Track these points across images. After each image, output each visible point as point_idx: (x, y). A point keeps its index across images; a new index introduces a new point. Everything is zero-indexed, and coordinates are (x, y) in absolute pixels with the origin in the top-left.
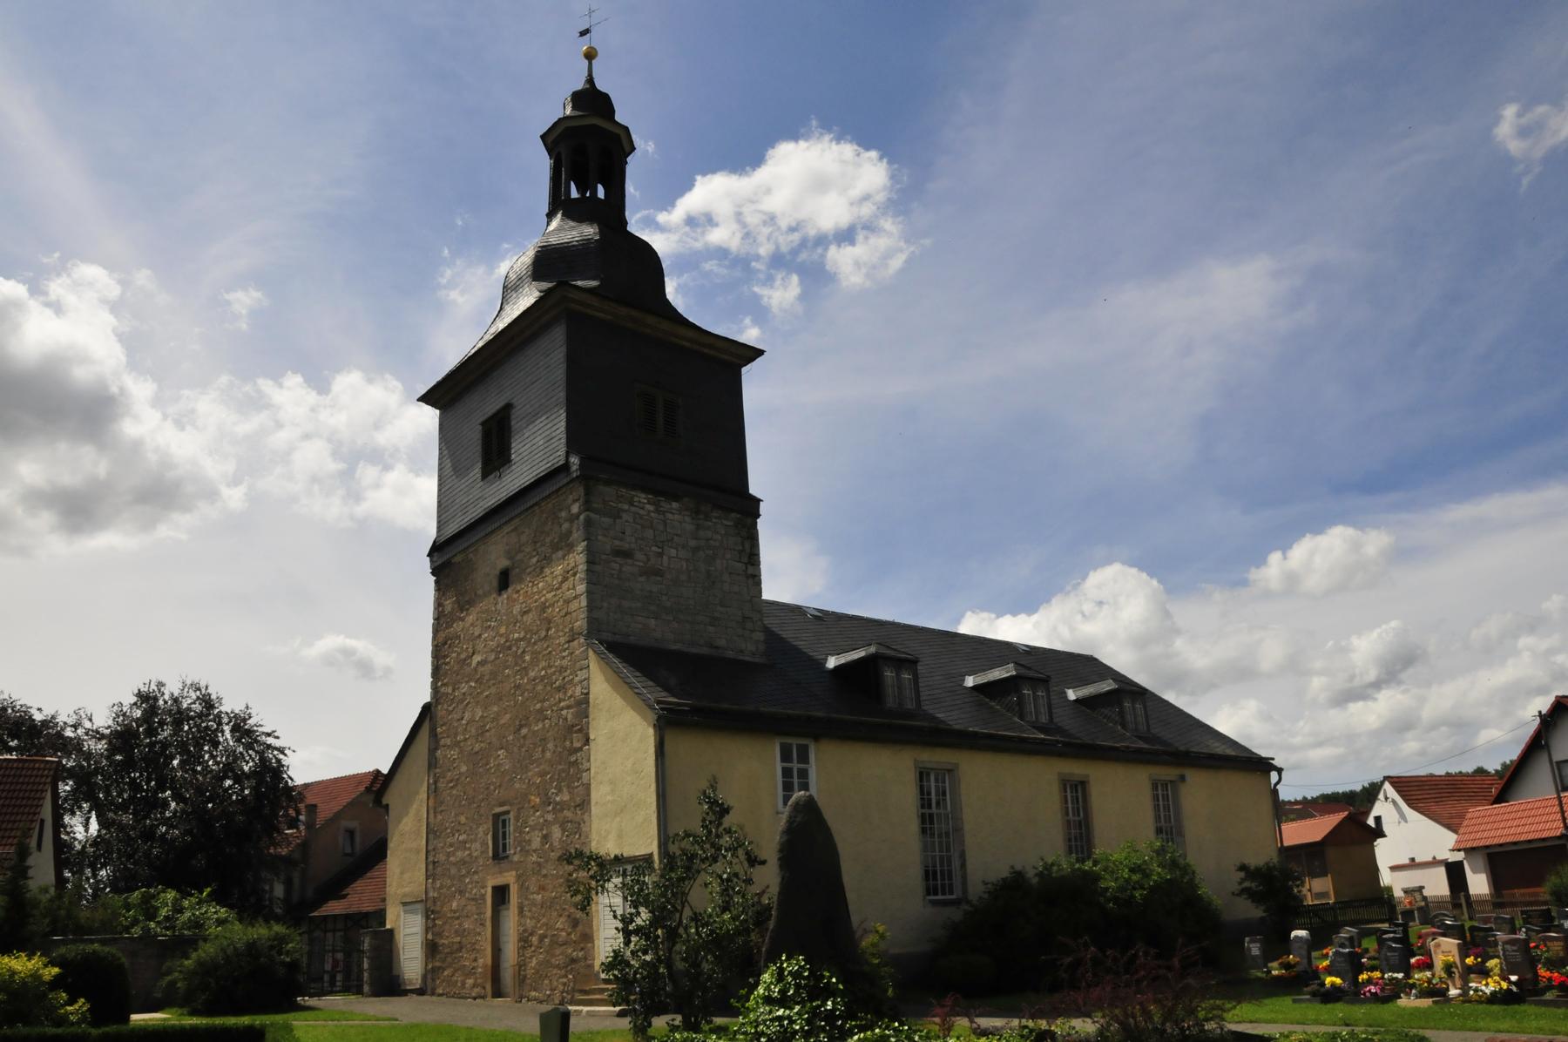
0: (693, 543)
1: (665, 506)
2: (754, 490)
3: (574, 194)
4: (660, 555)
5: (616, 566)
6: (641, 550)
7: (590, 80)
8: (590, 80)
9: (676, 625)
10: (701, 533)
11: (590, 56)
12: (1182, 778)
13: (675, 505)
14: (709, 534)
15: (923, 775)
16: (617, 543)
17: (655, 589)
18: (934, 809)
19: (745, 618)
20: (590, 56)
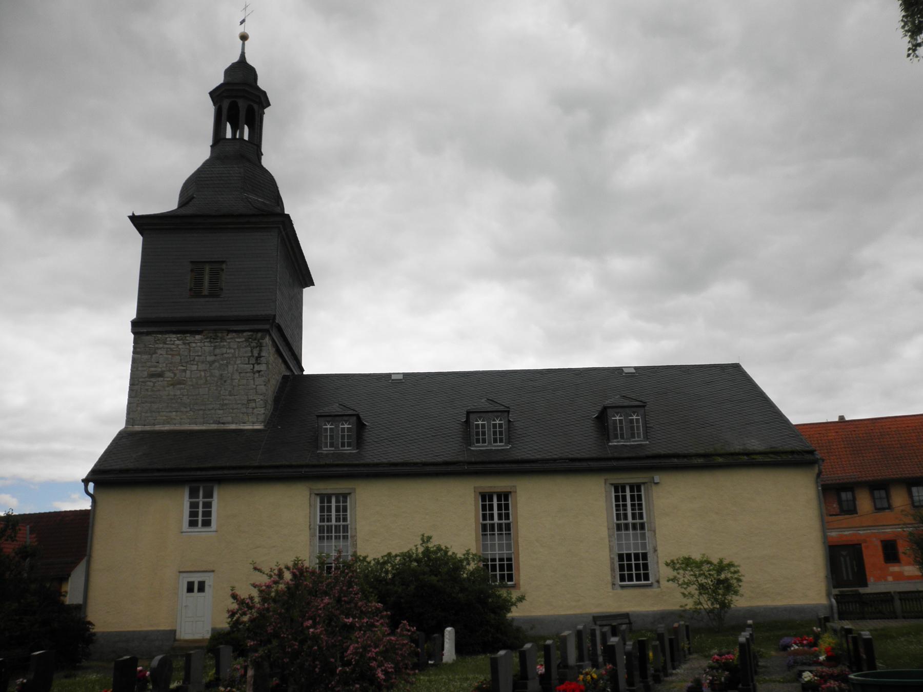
0: (210, 359)
1: (189, 338)
2: (132, 336)
3: (229, 135)
4: (185, 371)
5: (151, 384)
6: (170, 371)
7: (243, 55)
8: (243, 55)
9: (192, 413)
10: (218, 351)
11: (244, 37)
12: (354, 489)
13: (198, 337)
14: (224, 350)
15: (486, 497)
16: (153, 369)
17: (178, 393)
18: (334, 522)
19: (249, 401)
20: (244, 37)
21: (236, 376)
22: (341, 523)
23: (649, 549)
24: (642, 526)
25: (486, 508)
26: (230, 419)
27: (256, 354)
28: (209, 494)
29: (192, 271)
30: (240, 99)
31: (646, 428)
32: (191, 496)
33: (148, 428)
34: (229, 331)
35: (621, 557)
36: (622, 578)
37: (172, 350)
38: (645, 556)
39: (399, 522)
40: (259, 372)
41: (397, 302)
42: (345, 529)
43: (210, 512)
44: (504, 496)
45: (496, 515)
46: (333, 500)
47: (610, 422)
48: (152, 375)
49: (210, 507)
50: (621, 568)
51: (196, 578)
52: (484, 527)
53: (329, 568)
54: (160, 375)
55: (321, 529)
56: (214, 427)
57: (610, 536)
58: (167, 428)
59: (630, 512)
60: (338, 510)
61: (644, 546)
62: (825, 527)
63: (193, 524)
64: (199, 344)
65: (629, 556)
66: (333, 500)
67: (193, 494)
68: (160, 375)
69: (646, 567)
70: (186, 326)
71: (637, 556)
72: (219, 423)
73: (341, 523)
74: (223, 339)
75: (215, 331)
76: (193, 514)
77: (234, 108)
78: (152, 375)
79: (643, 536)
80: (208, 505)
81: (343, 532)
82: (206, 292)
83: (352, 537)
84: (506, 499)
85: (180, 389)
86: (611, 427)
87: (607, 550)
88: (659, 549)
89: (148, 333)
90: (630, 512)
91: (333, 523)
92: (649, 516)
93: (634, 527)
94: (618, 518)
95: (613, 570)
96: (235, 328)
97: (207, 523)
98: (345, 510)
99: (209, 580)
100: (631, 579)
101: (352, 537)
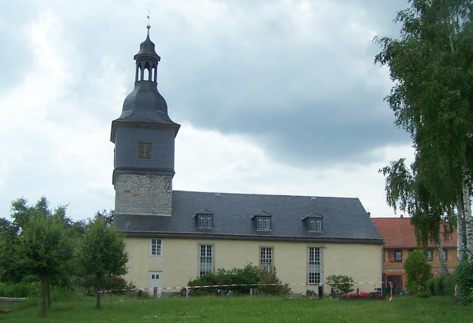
1: (141, 177)
7: (148, 37)
8: (148, 37)
10: (152, 183)
11: (149, 27)
13: (144, 176)
14: (155, 183)
15: (203, 247)
20: (149, 27)
21: (160, 194)
22: (209, 256)
23: (321, 272)
24: (319, 263)
25: (203, 251)
26: (158, 212)
27: (168, 185)
28: (159, 243)
29: (139, 146)
30: (147, 58)
31: (322, 228)
32: (153, 243)
33: (125, 213)
34: (157, 175)
35: (310, 274)
36: (310, 282)
37: (133, 181)
38: (319, 274)
39: (234, 257)
40: (169, 193)
41: (208, 162)
42: (210, 258)
43: (153, 247)
44: (210, 247)
45: (266, 255)
46: (266, 250)
47: (309, 224)
48: (126, 191)
49: (160, 248)
50: (310, 278)
51: (155, 274)
52: (261, 260)
53: (204, 273)
54: (129, 192)
55: (201, 258)
56: (152, 214)
57: (307, 266)
58: (132, 214)
59: (315, 257)
60: (208, 251)
61: (319, 270)
62: (384, 267)
63: (154, 253)
64: (144, 179)
65: (313, 274)
66: (266, 250)
67: (154, 242)
68: (129, 192)
69: (319, 278)
70: (139, 171)
71: (316, 274)
72: (153, 213)
73: (209, 256)
74: (154, 178)
75: (151, 174)
76: (154, 250)
77: (143, 63)
78: (126, 191)
79: (319, 267)
80: (159, 247)
81: (210, 260)
82: (145, 156)
83: (213, 261)
84: (270, 250)
85: (137, 198)
86: (309, 226)
87: (306, 271)
88: (324, 272)
89: (123, 174)
90: (315, 257)
91: (206, 254)
92: (321, 260)
93: (316, 263)
94: (310, 260)
95: (307, 278)
96: (160, 174)
97: (159, 254)
98: (270, 253)
99: (160, 275)
100: (313, 282)
101: (213, 261)
